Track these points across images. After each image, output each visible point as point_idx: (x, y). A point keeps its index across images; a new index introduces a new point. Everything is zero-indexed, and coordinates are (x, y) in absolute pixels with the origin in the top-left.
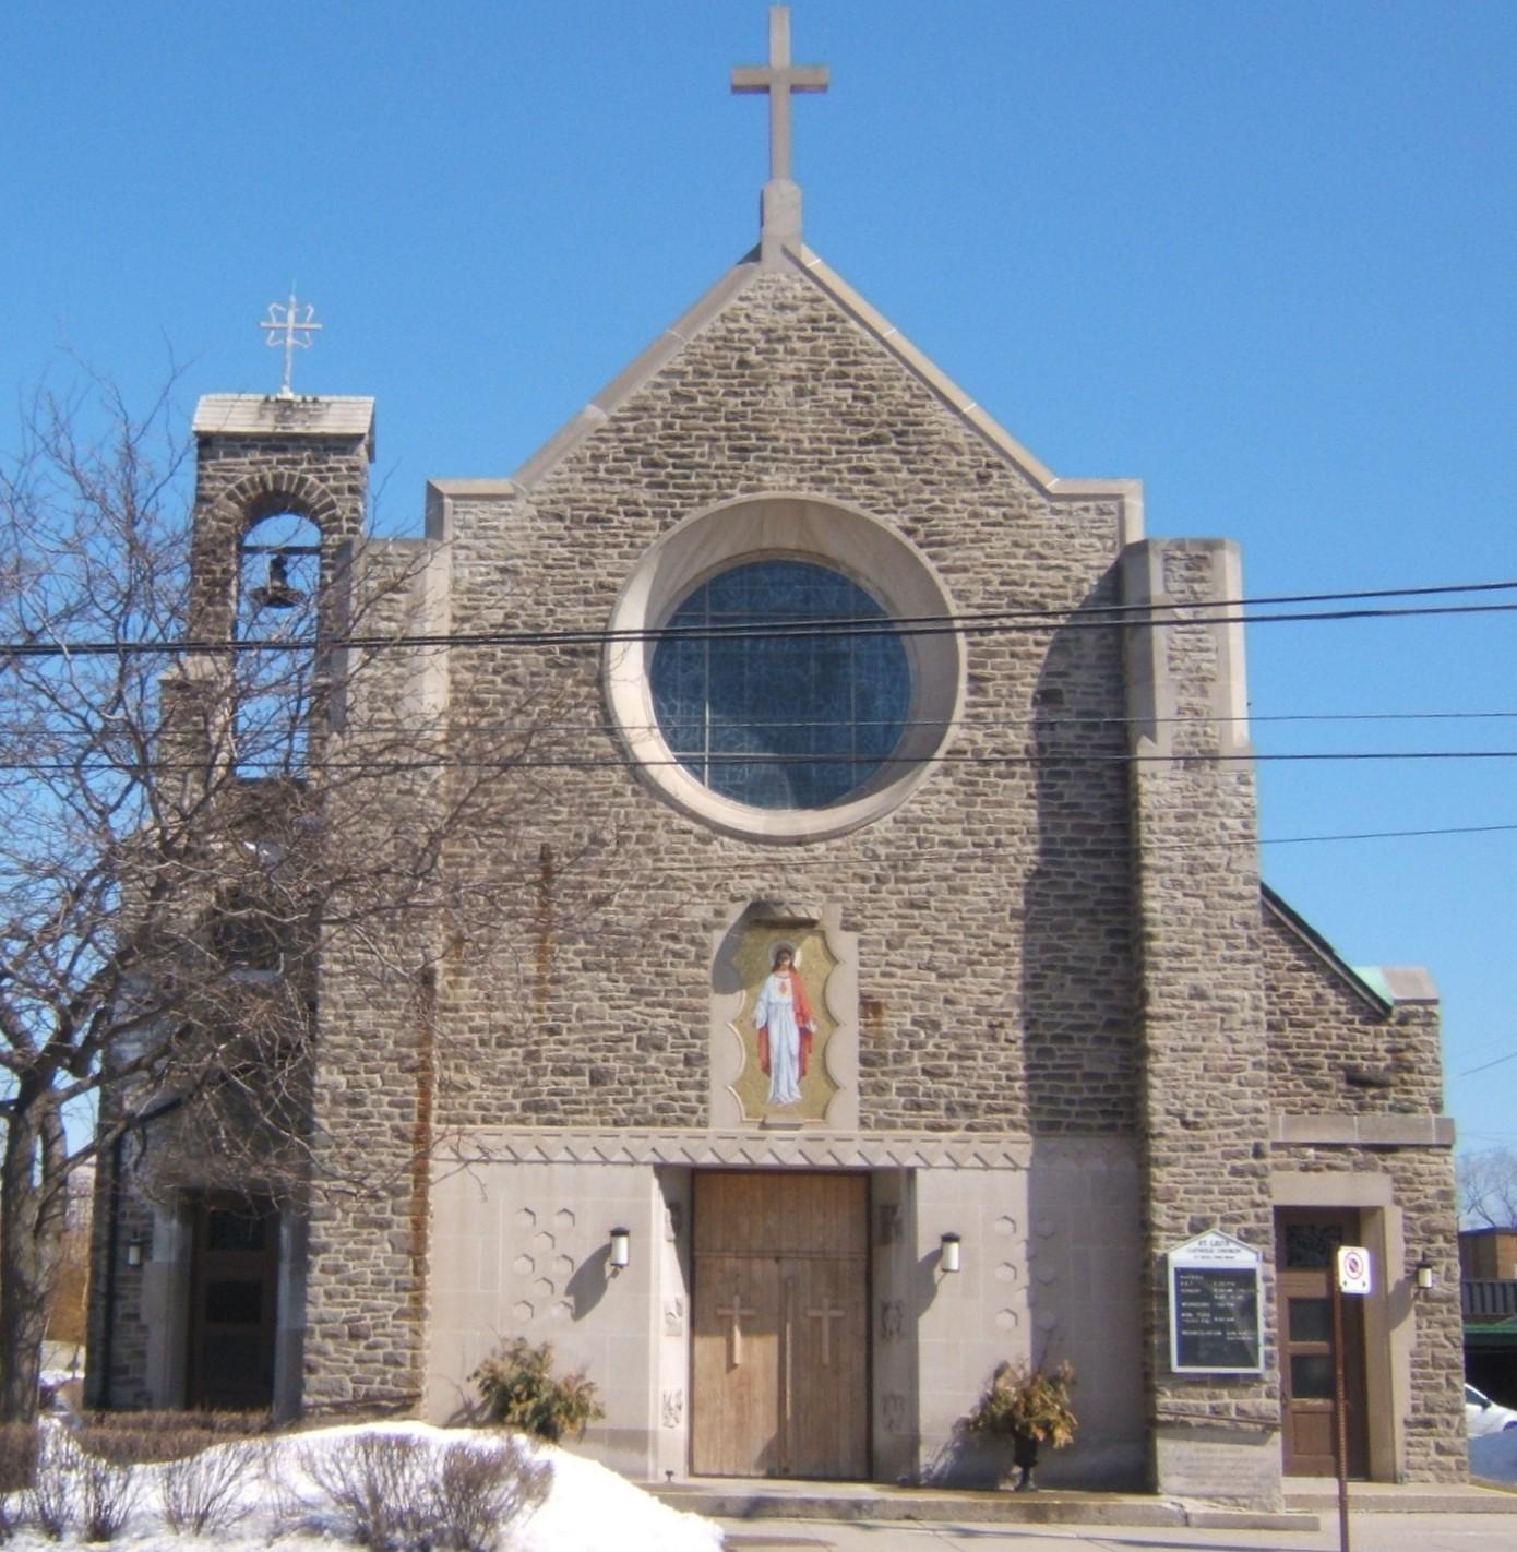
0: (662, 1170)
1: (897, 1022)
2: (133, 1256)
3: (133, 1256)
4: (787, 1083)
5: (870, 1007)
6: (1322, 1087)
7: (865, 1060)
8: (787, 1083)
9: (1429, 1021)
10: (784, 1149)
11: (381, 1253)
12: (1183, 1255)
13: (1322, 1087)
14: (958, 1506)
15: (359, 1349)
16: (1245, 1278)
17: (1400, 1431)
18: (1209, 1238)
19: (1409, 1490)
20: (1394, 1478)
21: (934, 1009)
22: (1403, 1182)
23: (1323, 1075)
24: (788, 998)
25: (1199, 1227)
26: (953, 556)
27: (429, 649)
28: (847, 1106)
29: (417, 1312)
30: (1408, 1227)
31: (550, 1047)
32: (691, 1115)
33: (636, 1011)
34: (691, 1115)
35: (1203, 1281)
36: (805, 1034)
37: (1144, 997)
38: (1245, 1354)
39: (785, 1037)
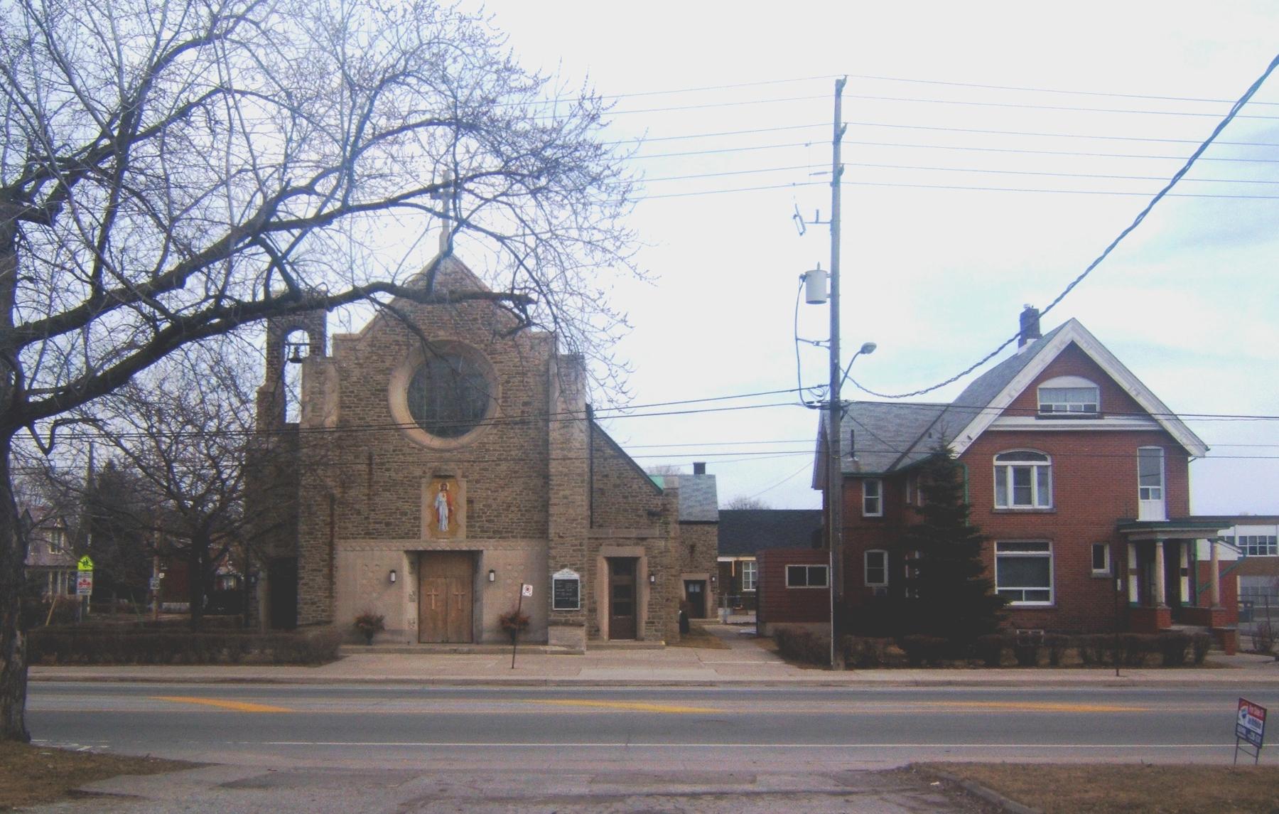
0: (407, 552)
1: (478, 506)
2: (253, 579)
3: (253, 579)
4: (444, 524)
5: (470, 501)
6: (640, 516)
7: (468, 517)
8: (444, 524)
9: (676, 495)
10: (443, 544)
11: (320, 579)
12: (557, 576)
13: (640, 516)
14: (757, 666)
15: (314, 607)
16: (575, 581)
17: (643, 624)
18: (566, 570)
19: (646, 643)
20: (642, 640)
21: (490, 501)
22: (648, 549)
23: (640, 512)
24: (444, 499)
25: (563, 567)
26: (499, 358)
27: (493, 170)
28: (462, 533)
29: (331, 597)
30: (649, 563)
31: (372, 515)
32: (416, 535)
33: (400, 504)
34: (416, 535)
35: (562, 583)
36: (450, 510)
37: (549, 498)
38: (574, 604)
39: (444, 511)
